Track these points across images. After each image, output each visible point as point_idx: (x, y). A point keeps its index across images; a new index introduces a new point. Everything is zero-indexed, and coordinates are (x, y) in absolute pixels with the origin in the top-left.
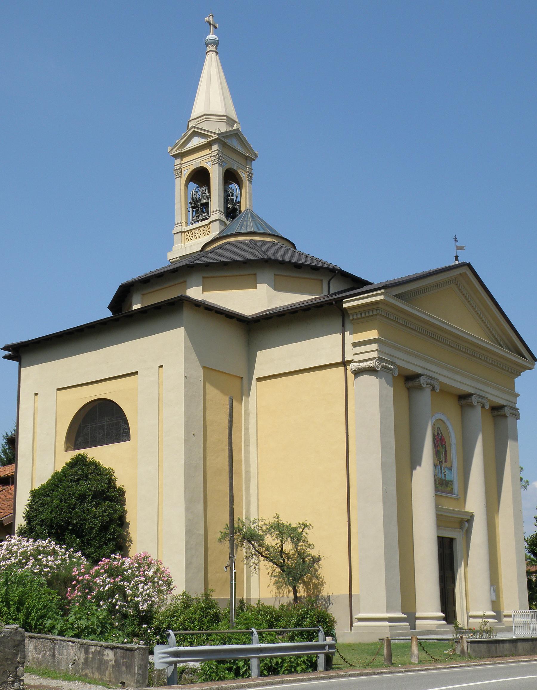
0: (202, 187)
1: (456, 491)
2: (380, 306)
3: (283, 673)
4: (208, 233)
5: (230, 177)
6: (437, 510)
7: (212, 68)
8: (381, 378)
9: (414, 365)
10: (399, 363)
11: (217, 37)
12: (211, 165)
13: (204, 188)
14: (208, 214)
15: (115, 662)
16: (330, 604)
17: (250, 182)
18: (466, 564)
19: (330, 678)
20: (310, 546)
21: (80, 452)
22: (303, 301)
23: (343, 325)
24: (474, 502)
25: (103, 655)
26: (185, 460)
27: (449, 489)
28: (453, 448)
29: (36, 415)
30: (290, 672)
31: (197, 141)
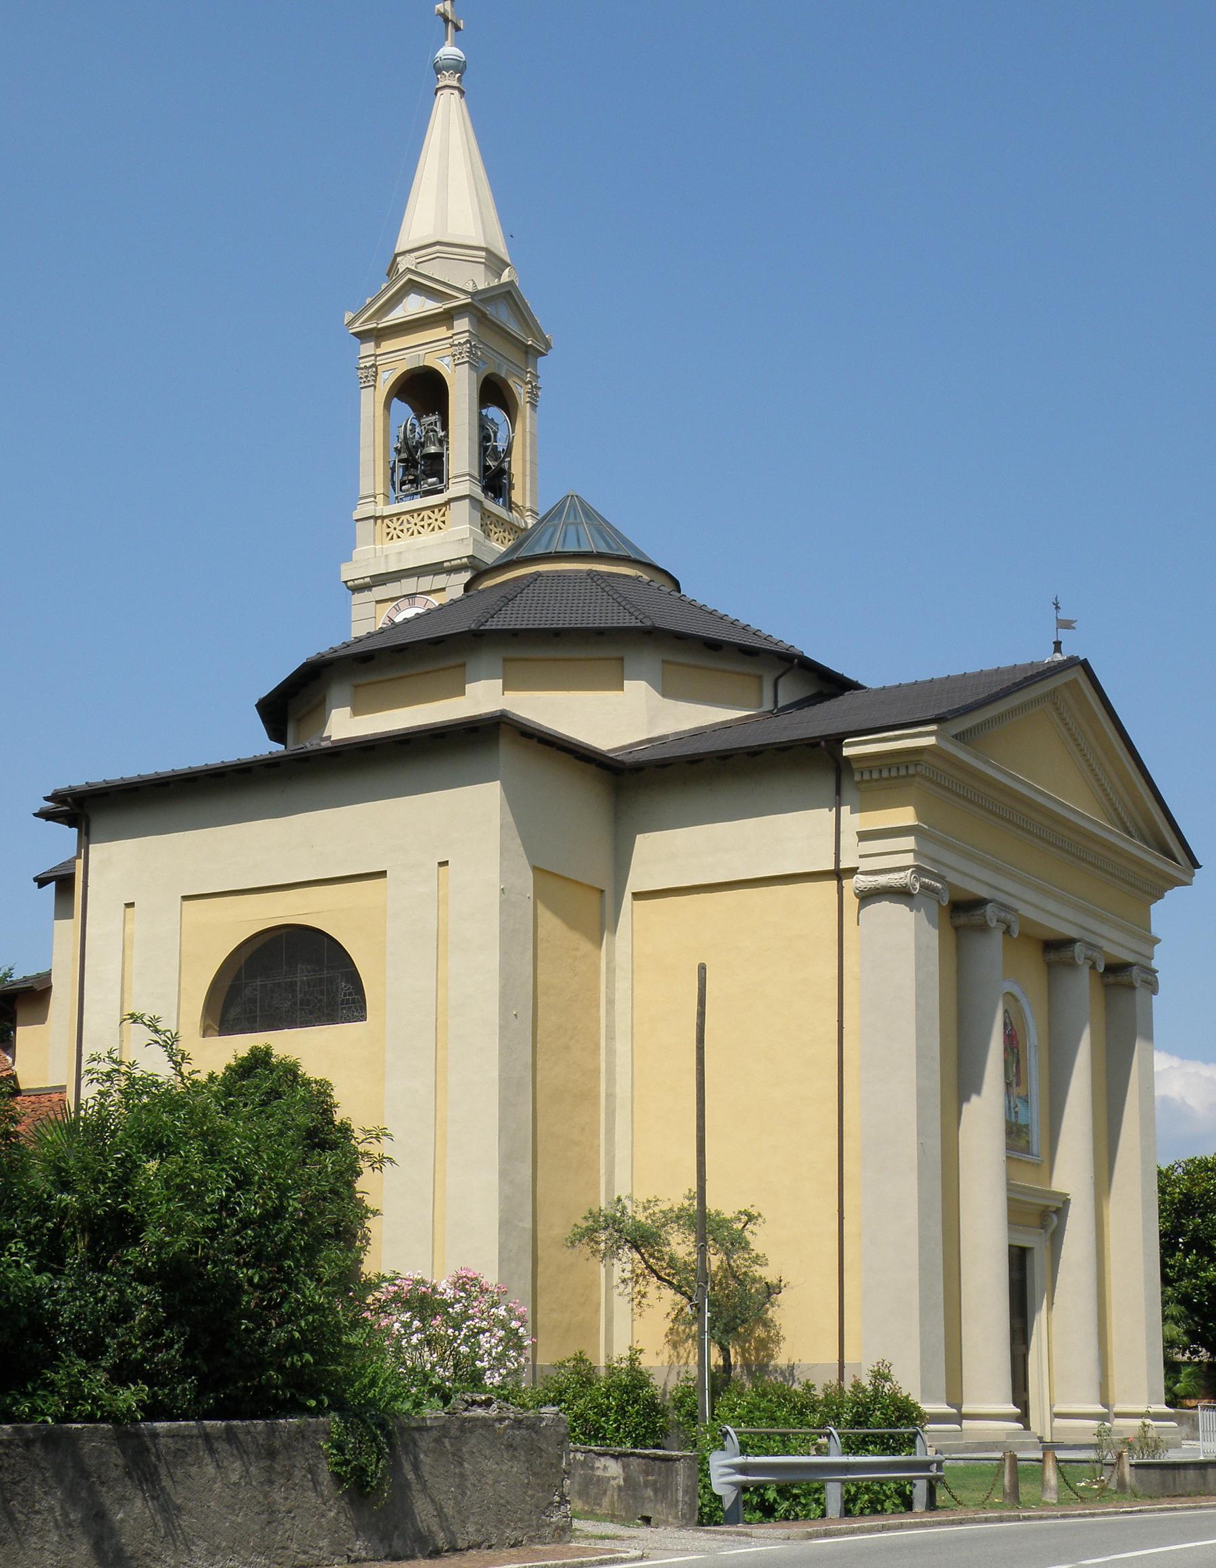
0: (428, 416)
1: (1035, 1150)
2: (926, 757)
3: (862, 1513)
4: (442, 525)
5: (493, 392)
6: (1008, 1190)
7: (449, 124)
8: (919, 911)
9: (975, 881)
10: (952, 877)
11: (462, 54)
12: (452, 364)
13: (433, 418)
14: (442, 482)
15: (625, 1480)
16: (794, 1381)
17: (534, 407)
18: (1051, 1304)
19: (853, 1532)
20: (757, 1260)
21: (259, 1039)
22: (723, 723)
23: (838, 792)
24: (1070, 1172)
25: (593, 1468)
26: (501, 1071)
27: (1023, 1143)
28: (1033, 1053)
29: (127, 952)
30: (875, 1512)
31: (415, 306)
